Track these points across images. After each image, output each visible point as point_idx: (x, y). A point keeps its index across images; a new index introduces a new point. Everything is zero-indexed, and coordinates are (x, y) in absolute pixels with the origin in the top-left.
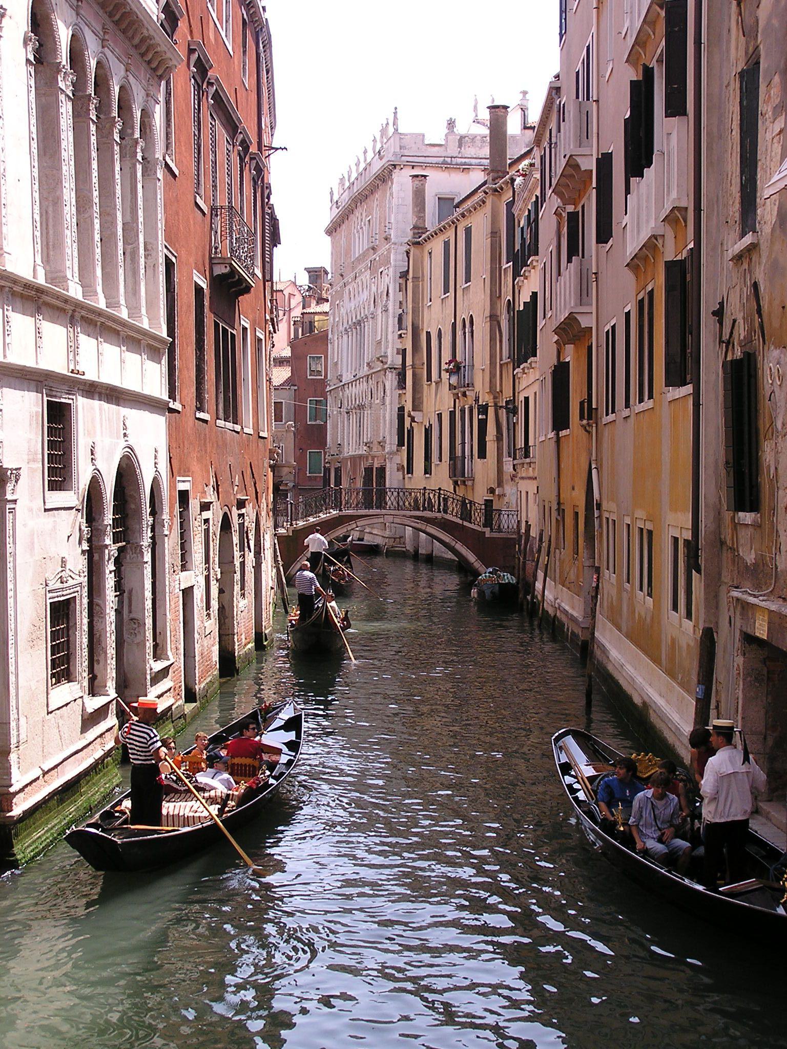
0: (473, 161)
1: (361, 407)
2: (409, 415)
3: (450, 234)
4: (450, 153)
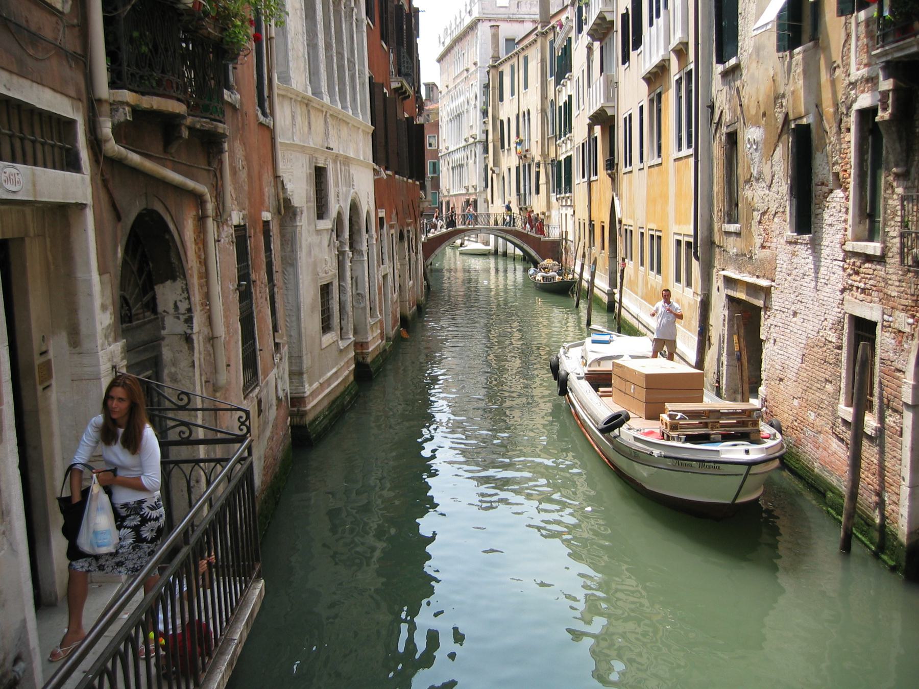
0: (526, 16)
1: (461, 166)
2: (491, 169)
3: (515, 60)
4: (512, 11)
